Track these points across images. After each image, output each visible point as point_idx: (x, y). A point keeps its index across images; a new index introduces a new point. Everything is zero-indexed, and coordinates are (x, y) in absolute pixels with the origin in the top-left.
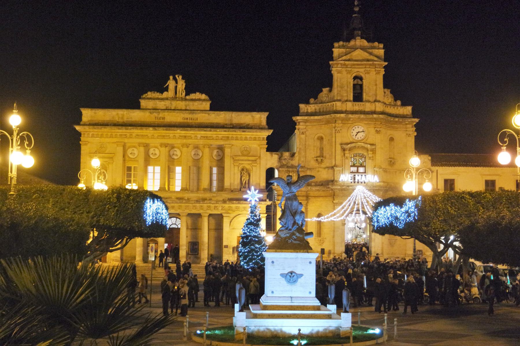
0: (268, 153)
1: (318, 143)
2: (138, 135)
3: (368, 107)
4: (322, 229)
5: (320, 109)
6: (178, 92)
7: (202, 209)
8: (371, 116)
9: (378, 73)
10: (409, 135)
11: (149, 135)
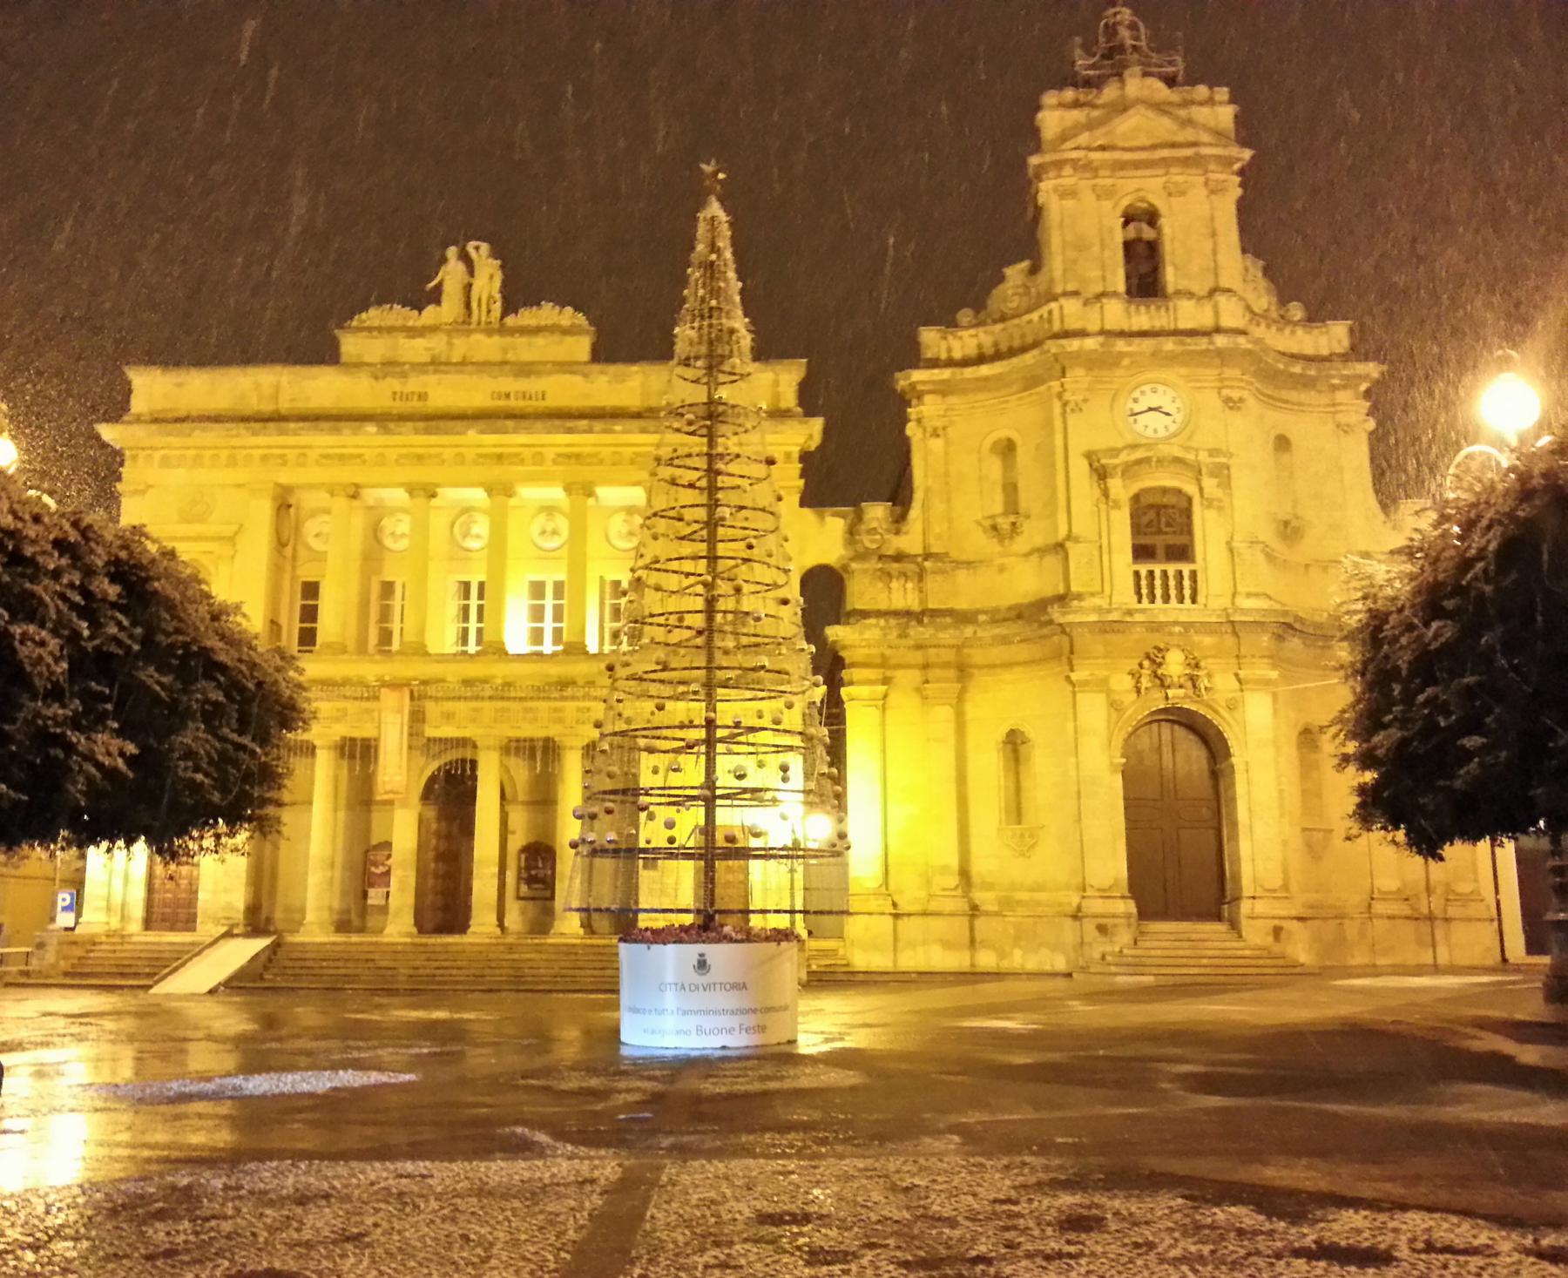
0: (806, 510)
1: (995, 468)
2: (327, 457)
3: (1188, 314)
4: (1024, 794)
5: (996, 344)
6: (474, 305)
7: (561, 721)
8: (1202, 344)
9: (1214, 190)
10: (1345, 429)
11: (369, 454)
